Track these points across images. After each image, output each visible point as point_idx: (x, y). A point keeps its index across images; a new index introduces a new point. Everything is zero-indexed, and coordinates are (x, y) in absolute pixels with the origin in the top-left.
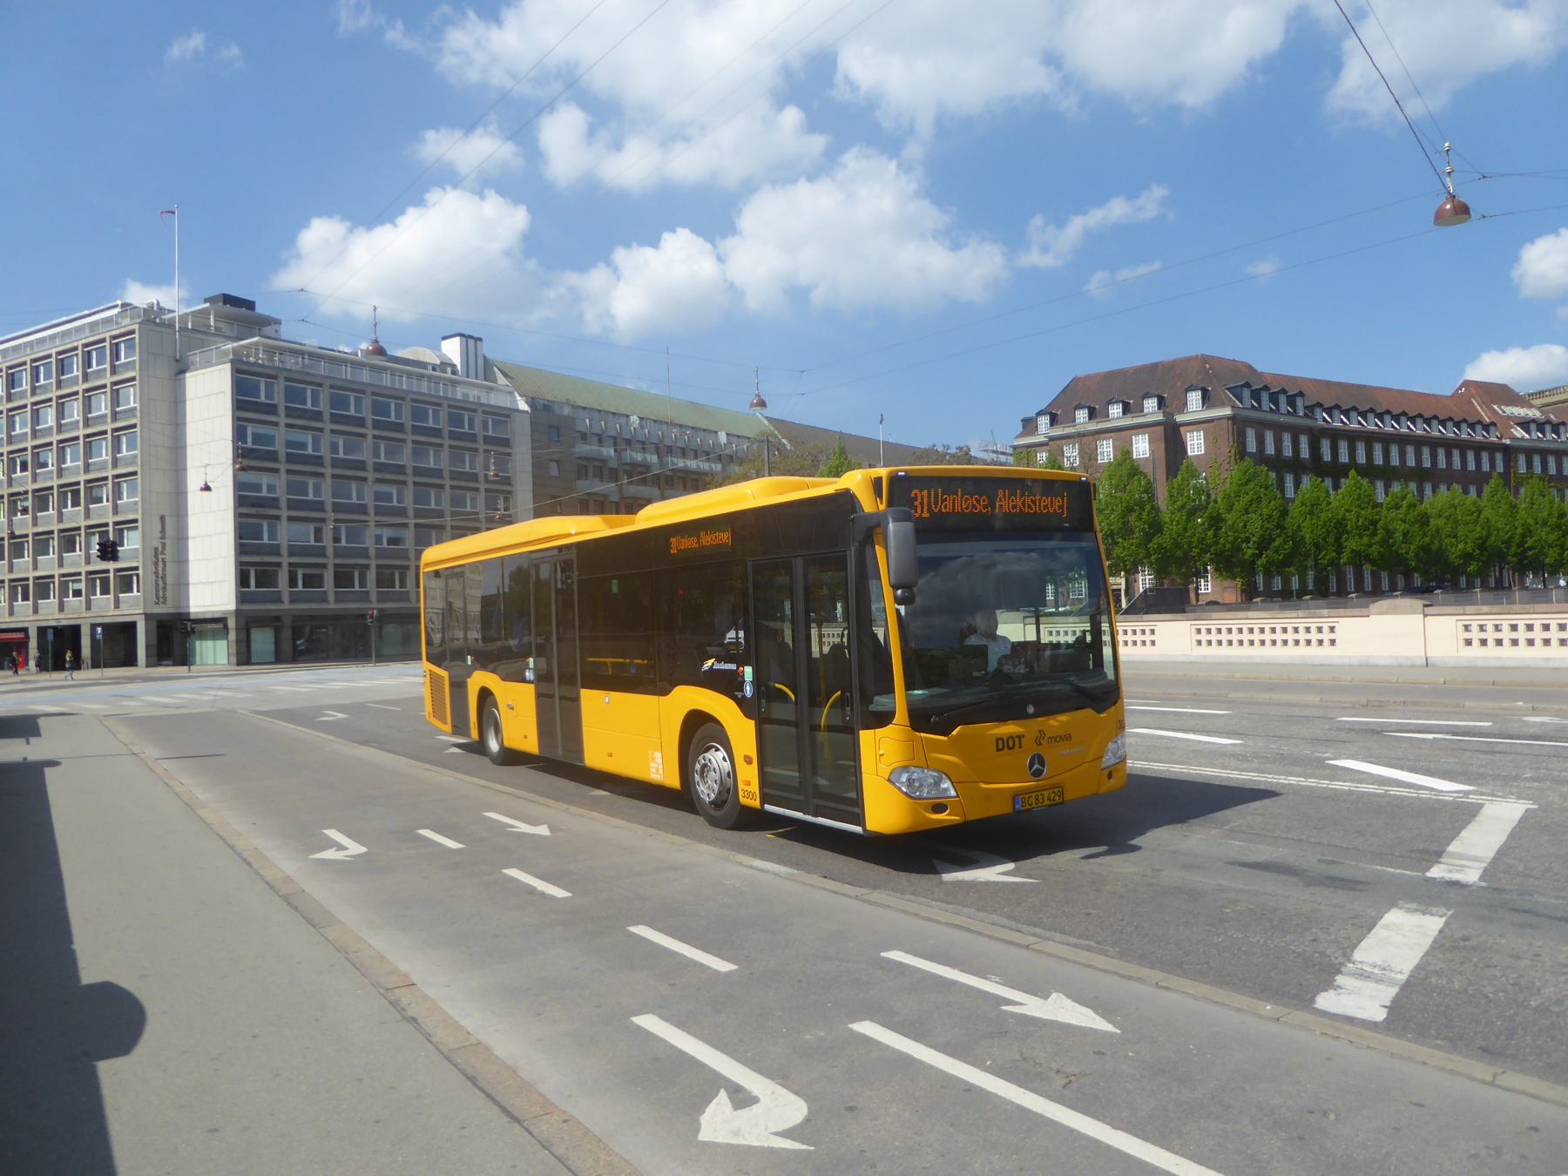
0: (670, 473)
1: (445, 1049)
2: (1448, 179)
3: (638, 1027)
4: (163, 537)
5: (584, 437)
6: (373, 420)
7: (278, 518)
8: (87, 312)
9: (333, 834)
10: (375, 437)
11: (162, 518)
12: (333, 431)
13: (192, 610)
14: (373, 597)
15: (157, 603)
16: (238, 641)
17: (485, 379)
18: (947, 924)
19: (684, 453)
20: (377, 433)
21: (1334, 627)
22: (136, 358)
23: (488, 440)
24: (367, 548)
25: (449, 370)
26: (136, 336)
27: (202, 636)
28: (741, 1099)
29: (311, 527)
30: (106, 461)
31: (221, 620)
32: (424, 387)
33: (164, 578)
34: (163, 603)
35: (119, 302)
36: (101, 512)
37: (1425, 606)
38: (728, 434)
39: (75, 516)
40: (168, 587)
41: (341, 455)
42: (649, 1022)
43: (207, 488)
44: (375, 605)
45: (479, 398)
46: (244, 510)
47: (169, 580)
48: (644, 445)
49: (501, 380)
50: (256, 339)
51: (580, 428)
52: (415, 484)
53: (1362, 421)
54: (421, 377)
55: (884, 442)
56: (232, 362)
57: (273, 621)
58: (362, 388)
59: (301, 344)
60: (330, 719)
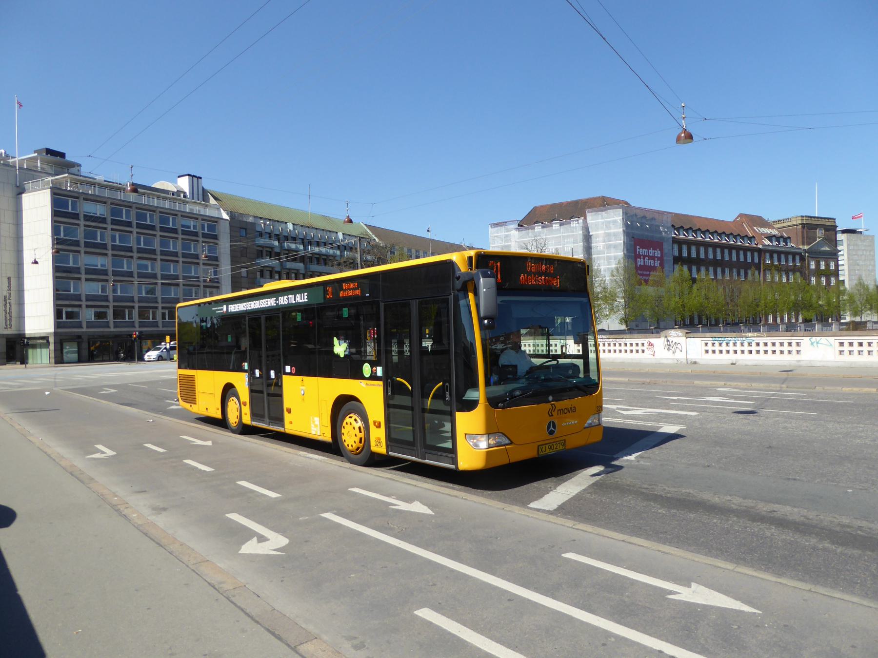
0: (311, 255)
1: (136, 525)
2: (683, 121)
3: (228, 517)
4: (10, 289)
5: (261, 234)
6: (137, 223)
7: (79, 279)
9: (100, 447)
10: (137, 233)
11: (9, 279)
12: (112, 229)
13: (27, 332)
14: (137, 325)
15: (5, 328)
16: (55, 350)
18: (387, 478)
19: (318, 244)
21: (708, 343)
23: (204, 236)
25: (182, 195)
27: (34, 347)
28: (262, 539)
29: (100, 284)
31: (46, 338)
32: (167, 204)
33: (10, 313)
34: (10, 328)
37: (687, 333)
38: (343, 234)
41: (117, 243)
42: (235, 517)
43: (36, 262)
44: (138, 329)
45: (199, 211)
46: (59, 274)
47: (14, 314)
48: (294, 239)
49: (212, 201)
50: (66, 175)
51: (258, 229)
52: (162, 260)
53: (686, 234)
55: (432, 240)
56: (51, 188)
57: (77, 339)
58: (130, 204)
59: (93, 178)
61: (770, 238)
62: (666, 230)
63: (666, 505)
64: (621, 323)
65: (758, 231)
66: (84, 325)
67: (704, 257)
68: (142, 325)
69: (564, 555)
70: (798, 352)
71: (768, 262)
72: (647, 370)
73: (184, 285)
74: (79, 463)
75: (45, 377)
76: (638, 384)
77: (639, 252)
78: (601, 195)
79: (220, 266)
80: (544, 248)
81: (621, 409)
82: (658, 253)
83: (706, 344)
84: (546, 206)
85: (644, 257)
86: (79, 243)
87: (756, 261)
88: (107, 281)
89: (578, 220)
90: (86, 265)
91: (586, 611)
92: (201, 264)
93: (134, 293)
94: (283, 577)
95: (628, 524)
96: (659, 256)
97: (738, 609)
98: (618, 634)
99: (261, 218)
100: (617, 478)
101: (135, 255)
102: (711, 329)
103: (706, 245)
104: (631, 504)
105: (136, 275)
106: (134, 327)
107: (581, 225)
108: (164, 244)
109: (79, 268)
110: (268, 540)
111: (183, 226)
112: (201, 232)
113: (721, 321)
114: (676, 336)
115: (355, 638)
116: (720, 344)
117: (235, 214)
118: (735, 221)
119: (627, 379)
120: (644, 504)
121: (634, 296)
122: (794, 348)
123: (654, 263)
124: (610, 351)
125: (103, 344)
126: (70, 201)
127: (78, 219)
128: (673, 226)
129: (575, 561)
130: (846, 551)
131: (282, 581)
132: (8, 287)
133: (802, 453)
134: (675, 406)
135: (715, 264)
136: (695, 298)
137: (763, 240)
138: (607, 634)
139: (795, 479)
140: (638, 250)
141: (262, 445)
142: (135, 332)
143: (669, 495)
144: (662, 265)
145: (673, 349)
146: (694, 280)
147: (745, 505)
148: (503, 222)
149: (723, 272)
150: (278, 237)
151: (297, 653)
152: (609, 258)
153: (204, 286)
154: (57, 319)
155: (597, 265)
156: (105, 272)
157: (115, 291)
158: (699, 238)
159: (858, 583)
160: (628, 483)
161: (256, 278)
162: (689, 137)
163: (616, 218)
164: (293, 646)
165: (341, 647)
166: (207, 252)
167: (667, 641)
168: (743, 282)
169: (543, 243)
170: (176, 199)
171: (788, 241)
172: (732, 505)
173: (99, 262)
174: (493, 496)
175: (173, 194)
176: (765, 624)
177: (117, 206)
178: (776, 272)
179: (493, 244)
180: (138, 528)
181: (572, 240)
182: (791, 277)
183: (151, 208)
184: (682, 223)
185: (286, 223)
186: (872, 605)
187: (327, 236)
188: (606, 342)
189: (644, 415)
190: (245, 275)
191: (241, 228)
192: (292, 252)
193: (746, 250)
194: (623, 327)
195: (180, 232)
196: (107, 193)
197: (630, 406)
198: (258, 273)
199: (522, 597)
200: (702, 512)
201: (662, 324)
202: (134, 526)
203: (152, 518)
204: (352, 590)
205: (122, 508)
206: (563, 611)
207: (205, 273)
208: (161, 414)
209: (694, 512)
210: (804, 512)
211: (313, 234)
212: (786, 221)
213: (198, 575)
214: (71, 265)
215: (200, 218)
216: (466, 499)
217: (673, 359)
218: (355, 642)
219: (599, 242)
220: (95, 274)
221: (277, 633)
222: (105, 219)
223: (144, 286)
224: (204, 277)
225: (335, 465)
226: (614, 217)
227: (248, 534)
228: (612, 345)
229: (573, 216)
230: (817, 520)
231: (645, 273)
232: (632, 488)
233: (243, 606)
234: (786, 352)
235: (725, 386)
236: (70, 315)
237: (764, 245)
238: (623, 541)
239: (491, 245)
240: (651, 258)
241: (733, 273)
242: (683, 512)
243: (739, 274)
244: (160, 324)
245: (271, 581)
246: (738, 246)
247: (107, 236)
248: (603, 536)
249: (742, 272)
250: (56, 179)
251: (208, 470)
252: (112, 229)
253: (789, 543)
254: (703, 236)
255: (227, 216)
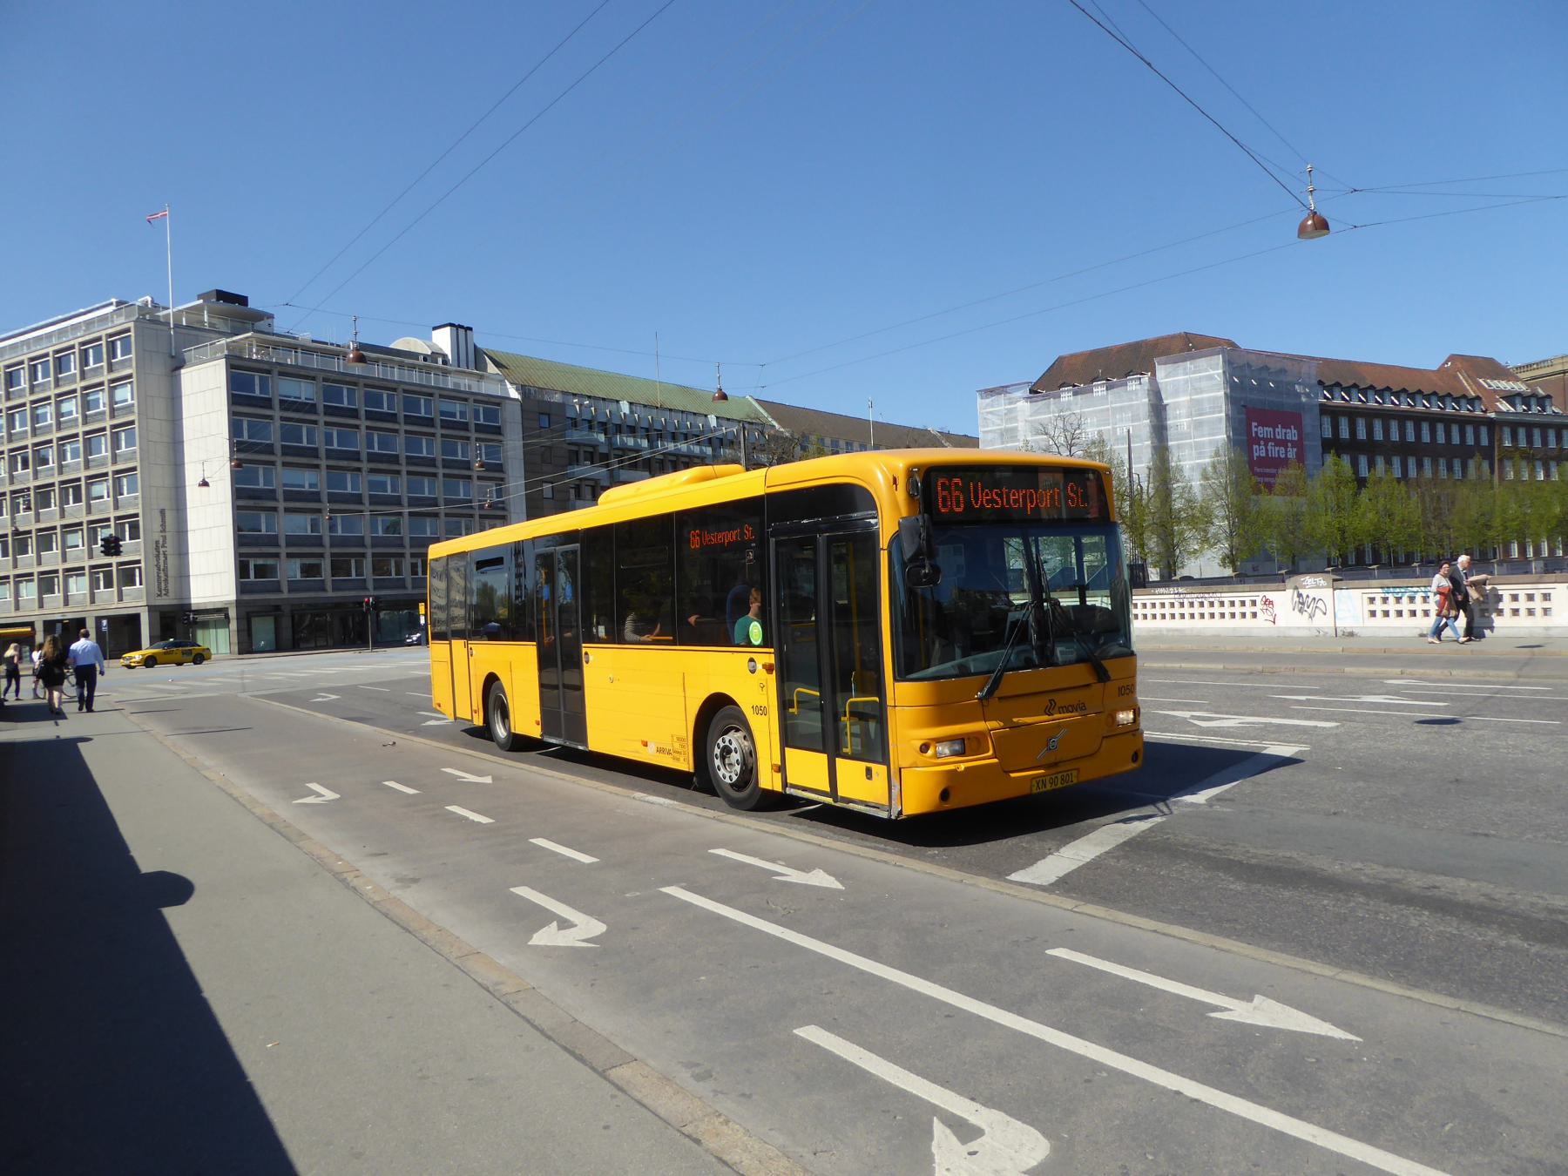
0: (662, 457)
4: (164, 531)
5: (575, 423)
7: (275, 509)
8: (82, 310)
9: (314, 786)
11: (162, 512)
12: (327, 424)
14: (370, 585)
15: (159, 595)
17: (476, 369)
19: (674, 437)
20: (369, 423)
21: (1387, 598)
22: (132, 356)
23: (479, 428)
24: (363, 537)
25: (440, 360)
26: (132, 334)
27: (205, 625)
28: (565, 924)
29: (309, 517)
30: (106, 457)
31: (223, 611)
32: (415, 377)
33: (165, 570)
34: (165, 594)
35: (114, 300)
36: (101, 507)
37: (1334, 580)
38: (717, 418)
39: (76, 512)
40: (169, 579)
41: (335, 446)
42: (523, 891)
43: (205, 484)
44: (372, 593)
45: (470, 387)
46: (241, 503)
47: (171, 572)
48: (632, 430)
50: (249, 334)
51: (570, 414)
52: (409, 473)
53: (1346, 397)
54: (413, 367)
55: (875, 423)
56: (227, 357)
57: (274, 610)
58: (353, 379)
59: (294, 338)
60: (324, 700)
61: (1510, 398)
62: (1307, 390)
63: (1245, 877)
64: (1223, 564)
65: (1487, 386)
66: (285, 588)
67: (1398, 440)
68: (378, 585)
69: (1048, 952)
70: (1546, 611)
71: (1507, 444)
72: (1260, 648)
73: (447, 515)
74: (283, 810)
75: (224, 675)
76: (1241, 674)
77: (1256, 433)
78: (1182, 331)
79: (506, 480)
80: (1077, 432)
81: (1199, 718)
82: (1292, 434)
83: (1372, 600)
84: (1082, 354)
85: (1266, 441)
86: (273, 449)
87: (1485, 441)
88: (319, 511)
89: (1140, 379)
90: (285, 485)
91: (1069, 1033)
92: (475, 478)
93: (364, 530)
94: (595, 980)
95: (1173, 908)
96: (1296, 439)
97: (1323, 1034)
98: (1115, 1066)
99: (574, 395)
100: (1168, 833)
101: (365, 466)
102: (1396, 572)
103: (1386, 416)
104: (1184, 875)
105: (366, 501)
106: (366, 589)
107: (1146, 388)
108: (412, 444)
109: (274, 491)
110: (576, 926)
111: (443, 413)
112: (472, 423)
113: (1418, 556)
114: (1315, 586)
115: (697, 1065)
116: (1398, 600)
117: (530, 390)
118: (1441, 370)
119: (1221, 666)
120: (1207, 876)
121: (1247, 514)
122: (1538, 604)
123: (1286, 452)
124: (1223, 615)
125: (317, 619)
126: (257, 376)
127: (270, 407)
128: (1320, 383)
129: (1066, 960)
130: (1546, 952)
131: (592, 985)
132: (162, 525)
133: (1513, 790)
134: (1298, 711)
135: (1404, 450)
136: (1365, 516)
137: (1498, 404)
138: (1096, 1066)
139: (1486, 835)
140: (1254, 429)
141: (574, 782)
142: (369, 597)
143: (1253, 861)
144: (1300, 458)
145: (1309, 610)
146: (1361, 483)
147: (1386, 876)
148: (1003, 387)
149: (1420, 466)
150: (604, 427)
151: (606, 1078)
152: (1198, 446)
153: (481, 517)
154: (241, 578)
155: (1175, 459)
156: (315, 497)
157: (332, 528)
158: (1372, 404)
159: (1552, 1001)
160: (1187, 841)
161: (569, 499)
162: (1322, 225)
163: (1212, 372)
164: (600, 1070)
165: (674, 1077)
166: (484, 457)
167: (1193, 1078)
168: (1459, 483)
169: (1075, 422)
170: (429, 367)
171: (1547, 402)
172: (1363, 878)
173: (306, 480)
174: (949, 863)
175: (425, 359)
176: (1364, 1056)
177: (333, 384)
178: (1524, 463)
179: (984, 427)
180: (374, 905)
181: (1130, 415)
182: (1554, 470)
183: (389, 385)
184: (1337, 376)
185: (618, 401)
186: (1558, 1032)
187: (688, 423)
188: (1185, 600)
189: (1238, 727)
190: (550, 496)
191: (542, 414)
192: (629, 453)
193: (1463, 422)
194: (1228, 572)
195: (438, 423)
196: (315, 362)
197: (1216, 713)
198: (572, 491)
199: (969, 1012)
200: (1306, 888)
201: (1302, 565)
202: (369, 903)
203: (398, 893)
204: (700, 999)
205: (349, 877)
206: (1030, 1033)
207: (481, 493)
208: (411, 734)
209: (1291, 888)
210: (1488, 888)
211: (665, 420)
212: (1525, 369)
213: (464, 972)
214: (261, 486)
215: (472, 398)
216: (901, 866)
217: (1309, 629)
218: (697, 1070)
219: (1180, 416)
220: (301, 500)
221: (577, 1052)
222: (314, 406)
223: (380, 518)
224: (480, 501)
225: (690, 813)
226: (1206, 370)
227: (543, 918)
228: (1196, 604)
229: (1131, 371)
230: (1507, 902)
231: (1267, 470)
232: (1191, 850)
233: (529, 1016)
234: (1539, 612)
235: (1401, 676)
236: (261, 571)
237: (1499, 412)
238: (1155, 931)
239: (981, 429)
240: (1279, 443)
241: (1437, 465)
242: (1271, 889)
243: (1450, 468)
244: (409, 584)
245: (576, 985)
246: (1464, 416)
247: (317, 435)
248: (1122, 924)
249: (1457, 464)
250: (234, 342)
251: (484, 822)
252: (327, 424)
253: (1447, 938)
254: (1379, 399)
255: (517, 393)
